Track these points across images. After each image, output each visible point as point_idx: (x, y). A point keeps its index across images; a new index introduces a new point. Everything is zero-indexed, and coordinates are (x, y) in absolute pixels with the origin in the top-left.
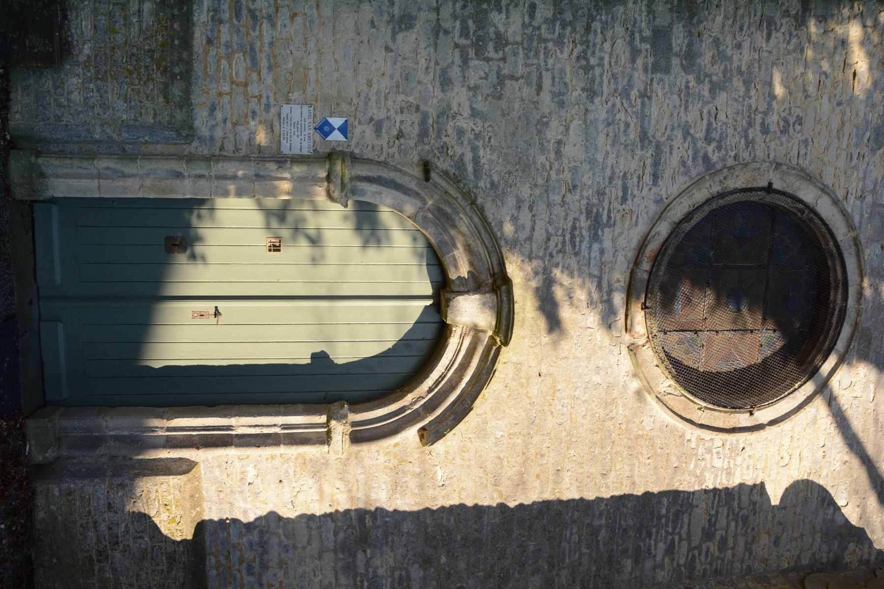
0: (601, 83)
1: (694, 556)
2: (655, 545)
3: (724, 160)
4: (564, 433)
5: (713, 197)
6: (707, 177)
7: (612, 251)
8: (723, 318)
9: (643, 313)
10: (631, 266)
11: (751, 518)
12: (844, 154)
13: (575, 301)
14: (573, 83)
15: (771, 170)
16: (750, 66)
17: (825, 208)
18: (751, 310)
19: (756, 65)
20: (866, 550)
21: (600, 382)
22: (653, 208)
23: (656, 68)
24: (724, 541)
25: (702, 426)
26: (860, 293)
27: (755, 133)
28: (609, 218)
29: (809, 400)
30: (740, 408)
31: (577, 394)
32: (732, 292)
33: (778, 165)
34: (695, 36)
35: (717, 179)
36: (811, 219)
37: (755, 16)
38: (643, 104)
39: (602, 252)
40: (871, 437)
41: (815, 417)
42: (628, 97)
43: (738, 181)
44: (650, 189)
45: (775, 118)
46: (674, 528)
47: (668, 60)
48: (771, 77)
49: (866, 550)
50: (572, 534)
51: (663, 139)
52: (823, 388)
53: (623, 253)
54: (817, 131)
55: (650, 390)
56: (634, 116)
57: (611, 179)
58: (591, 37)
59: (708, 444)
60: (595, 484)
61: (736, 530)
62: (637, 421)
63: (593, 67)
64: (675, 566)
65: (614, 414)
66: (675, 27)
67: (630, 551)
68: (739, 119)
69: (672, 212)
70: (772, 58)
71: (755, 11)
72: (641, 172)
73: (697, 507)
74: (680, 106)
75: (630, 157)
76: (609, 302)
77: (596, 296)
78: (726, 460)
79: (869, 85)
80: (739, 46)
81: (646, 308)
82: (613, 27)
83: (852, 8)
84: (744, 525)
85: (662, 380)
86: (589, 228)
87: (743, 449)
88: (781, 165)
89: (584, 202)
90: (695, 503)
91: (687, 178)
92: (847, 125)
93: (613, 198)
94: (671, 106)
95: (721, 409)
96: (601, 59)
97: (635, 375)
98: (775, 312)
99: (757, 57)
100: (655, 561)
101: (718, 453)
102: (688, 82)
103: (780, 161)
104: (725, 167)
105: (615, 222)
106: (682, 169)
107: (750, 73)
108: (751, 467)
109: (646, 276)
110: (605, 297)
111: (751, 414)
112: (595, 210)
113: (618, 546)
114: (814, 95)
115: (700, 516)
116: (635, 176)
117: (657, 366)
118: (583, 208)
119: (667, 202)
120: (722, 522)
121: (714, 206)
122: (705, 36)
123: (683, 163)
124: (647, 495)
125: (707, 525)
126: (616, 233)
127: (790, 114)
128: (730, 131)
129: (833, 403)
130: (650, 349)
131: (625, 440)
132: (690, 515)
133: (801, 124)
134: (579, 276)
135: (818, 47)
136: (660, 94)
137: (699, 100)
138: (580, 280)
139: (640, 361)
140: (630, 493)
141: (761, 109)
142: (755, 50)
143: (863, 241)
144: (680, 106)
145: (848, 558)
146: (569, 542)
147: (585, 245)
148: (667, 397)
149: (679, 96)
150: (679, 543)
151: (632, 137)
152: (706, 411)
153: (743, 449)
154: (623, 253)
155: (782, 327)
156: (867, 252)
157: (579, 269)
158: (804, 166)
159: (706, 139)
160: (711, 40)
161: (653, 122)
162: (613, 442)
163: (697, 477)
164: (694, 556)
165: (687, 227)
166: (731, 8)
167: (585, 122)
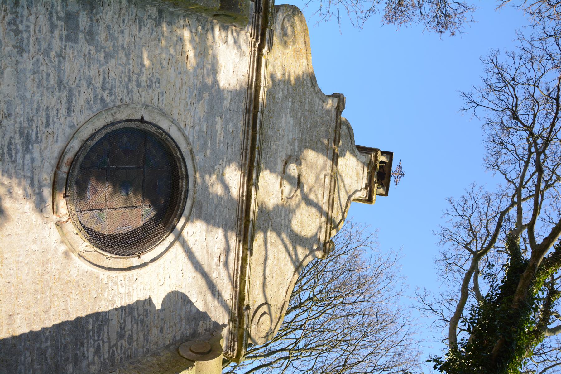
0: (28, 44)
1: (113, 351)
2: (87, 350)
3: (114, 101)
4: (13, 288)
5: (108, 125)
6: (104, 112)
7: (40, 160)
8: (119, 200)
9: (65, 200)
10: (55, 169)
11: (145, 319)
12: (183, 101)
13: (14, 195)
14: (6, 41)
15: (143, 109)
16: (129, 45)
17: (174, 133)
18: (135, 194)
19: (133, 45)
20: (208, 323)
21: (37, 249)
22: (68, 131)
23: (68, 38)
24: (131, 337)
25: (110, 269)
26: (195, 182)
27: (133, 86)
28: (37, 137)
29: (172, 245)
30: (132, 254)
31: (20, 259)
32: (122, 184)
33: (147, 106)
34: (94, 22)
35: (110, 113)
36: (167, 139)
37: (132, 15)
38: (59, 61)
39: (33, 160)
40: (206, 261)
41: (176, 254)
42: (48, 56)
43: (123, 115)
44: (66, 118)
45: (144, 78)
46: (99, 337)
47: (77, 35)
48: (142, 53)
49: (208, 323)
50: (25, 358)
51: (74, 86)
52: (179, 237)
53: (48, 161)
54: (168, 88)
55: (73, 250)
56: (53, 69)
57: (37, 110)
58: (19, 10)
59: (114, 280)
60: (40, 319)
61: (137, 329)
62: (66, 272)
63: (21, 32)
64: (102, 360)
65: (49, 269)
66: (81, 14)
67: (70, 359)
68: (123, 77)
69: (81, 133)
70: (143, 42)
71: (132, 12)
72: (59, 106)
73: (112, 320)
74: (85, 65)
75: (50, 97)
76: (40, 194)
77: (29, 190)
78: (127, 287)
79: (195, 65)
80: (122, 32)
81: (67, 196)
82: (36, 6)
83: (185, 20)
84: (142, 325)
85: (81, 243)
86: (22, 143)
87: (137, 279)
88: (148, 106)
89: (17, 126)
90: (110, 318)
91: (90, 112)
92: (184, 86)
93: (40, 123)
94: (79, 65)
95: (120, 256)
96: (28, 27)
97: (62, 242)
98: (149, 194)
99: (133, 40)
100: (88, 360)
101: (121, 284)
102: (90, 50)
103: (147, 104)
104: (114, 106)
105: (41, 140)
106: (87, 106)
107: (129, 49)
108: (142, 289)
109: (65, 176)
110: (37, 191)
111: (139, 257)
112: (26, 132)
113: (61, 358)
114: (166, 66)
115: (114, 325)
116: (55, 110)
117: (77, 234)
118: (17, 130)
119: (78, 127)
120: (128, 326)
121: (108, 130)
122: (101, 23)
123: (88, 103)
124: (79, 319)
125: (119, 330)
126: (43, 147)
127: (153, 76)
128: (118, 84)
129: (185, 245)
130: (71, 223)
131: (59, 286)
132: (108, 326)
133: (159, 83)
134: (16, 177)
135: (168, 39)
136: (71, 56)
137: (97, 63)
138: (17, 180)
139: (65, 232)
140: (66, 320)
141: (136, 72)
142: (132, 36)
143: (195, 152)
144: (85, 65)
145: (200, 330)
146: (24, 364)
147: (19, 156)
148: (85, 254)
149: (84, 59)
150: (103, 345)
151: (52, 83)
152: (112, 259)
153: (137, 279)
154: (48, 161)
155: (154, 203)
156: (197, 157)
157: (16, 172)
158: (162, 107)
159: (102, 88)
160: (105, 25)
161: (66, 74)
162: (51, 288)
163: (110, 301)
164: (113, 351)
165: (92, 143)
166: (117, 8)
167: (16, 69)
